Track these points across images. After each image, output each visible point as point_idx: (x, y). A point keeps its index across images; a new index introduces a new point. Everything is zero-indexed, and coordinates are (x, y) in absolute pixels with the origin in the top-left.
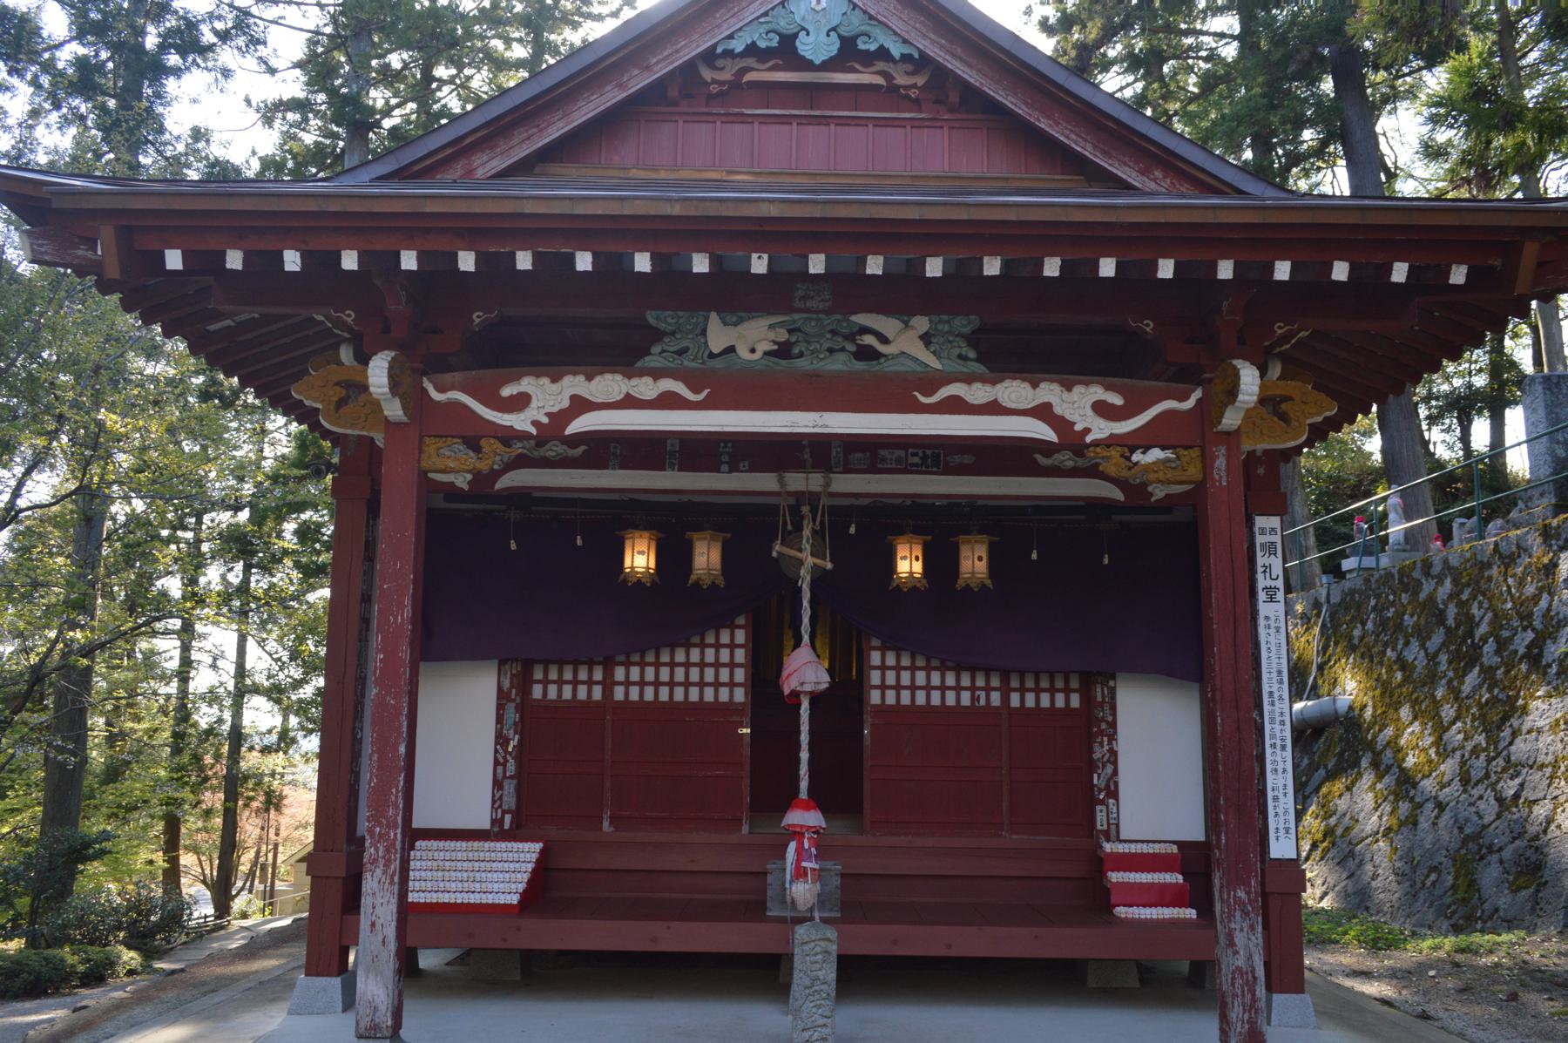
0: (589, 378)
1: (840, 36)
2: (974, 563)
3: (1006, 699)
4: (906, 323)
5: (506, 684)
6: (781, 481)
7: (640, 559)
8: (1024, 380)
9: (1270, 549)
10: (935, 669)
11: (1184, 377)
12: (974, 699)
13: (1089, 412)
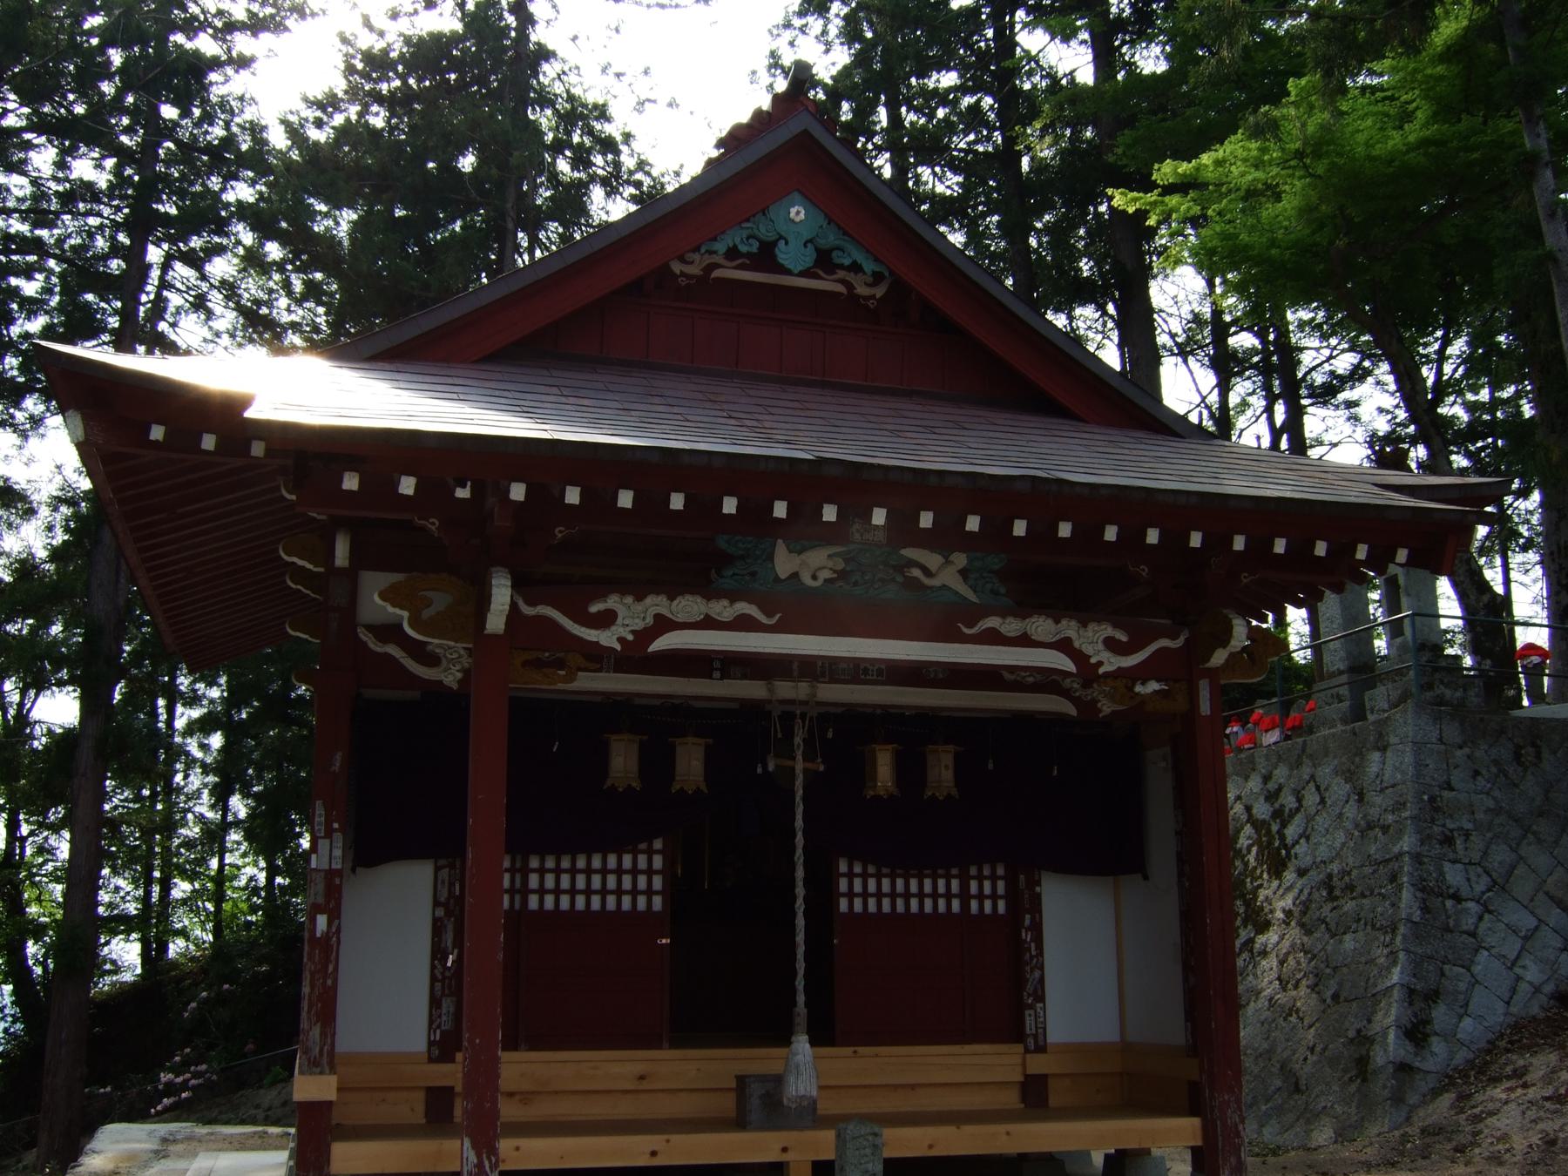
0: (672, 599)
1: (817, 249)
2: (942, 772)
3: (965, 906)
4: (946, 558)
6: (771, 690)
8: (1048, 616)
10: (886, 876)
13: (1100, 646)
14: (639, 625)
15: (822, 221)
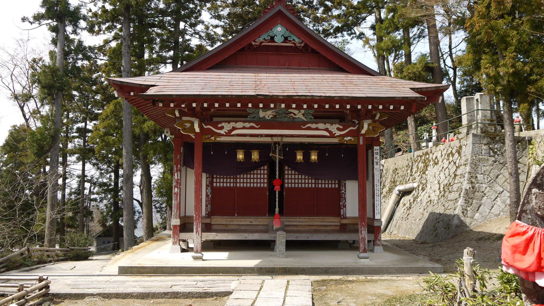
2: (314, 157)
5: (208, 183)
7: (240, 156)
9: (377, 153)
11: (354, 124)
12: (315, 186)
14: (229, 129)
15: (285, 30)
